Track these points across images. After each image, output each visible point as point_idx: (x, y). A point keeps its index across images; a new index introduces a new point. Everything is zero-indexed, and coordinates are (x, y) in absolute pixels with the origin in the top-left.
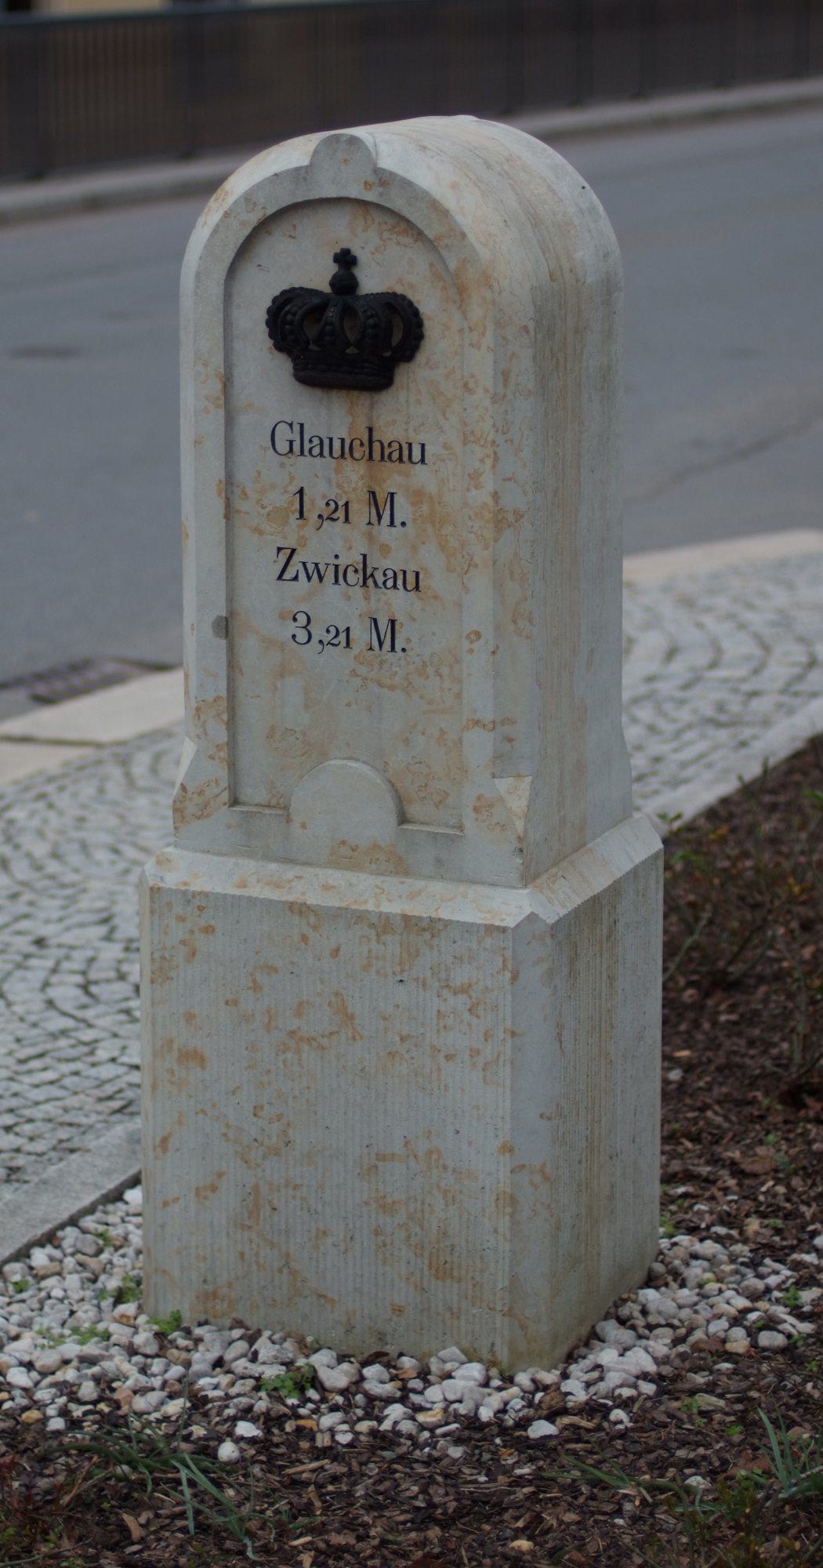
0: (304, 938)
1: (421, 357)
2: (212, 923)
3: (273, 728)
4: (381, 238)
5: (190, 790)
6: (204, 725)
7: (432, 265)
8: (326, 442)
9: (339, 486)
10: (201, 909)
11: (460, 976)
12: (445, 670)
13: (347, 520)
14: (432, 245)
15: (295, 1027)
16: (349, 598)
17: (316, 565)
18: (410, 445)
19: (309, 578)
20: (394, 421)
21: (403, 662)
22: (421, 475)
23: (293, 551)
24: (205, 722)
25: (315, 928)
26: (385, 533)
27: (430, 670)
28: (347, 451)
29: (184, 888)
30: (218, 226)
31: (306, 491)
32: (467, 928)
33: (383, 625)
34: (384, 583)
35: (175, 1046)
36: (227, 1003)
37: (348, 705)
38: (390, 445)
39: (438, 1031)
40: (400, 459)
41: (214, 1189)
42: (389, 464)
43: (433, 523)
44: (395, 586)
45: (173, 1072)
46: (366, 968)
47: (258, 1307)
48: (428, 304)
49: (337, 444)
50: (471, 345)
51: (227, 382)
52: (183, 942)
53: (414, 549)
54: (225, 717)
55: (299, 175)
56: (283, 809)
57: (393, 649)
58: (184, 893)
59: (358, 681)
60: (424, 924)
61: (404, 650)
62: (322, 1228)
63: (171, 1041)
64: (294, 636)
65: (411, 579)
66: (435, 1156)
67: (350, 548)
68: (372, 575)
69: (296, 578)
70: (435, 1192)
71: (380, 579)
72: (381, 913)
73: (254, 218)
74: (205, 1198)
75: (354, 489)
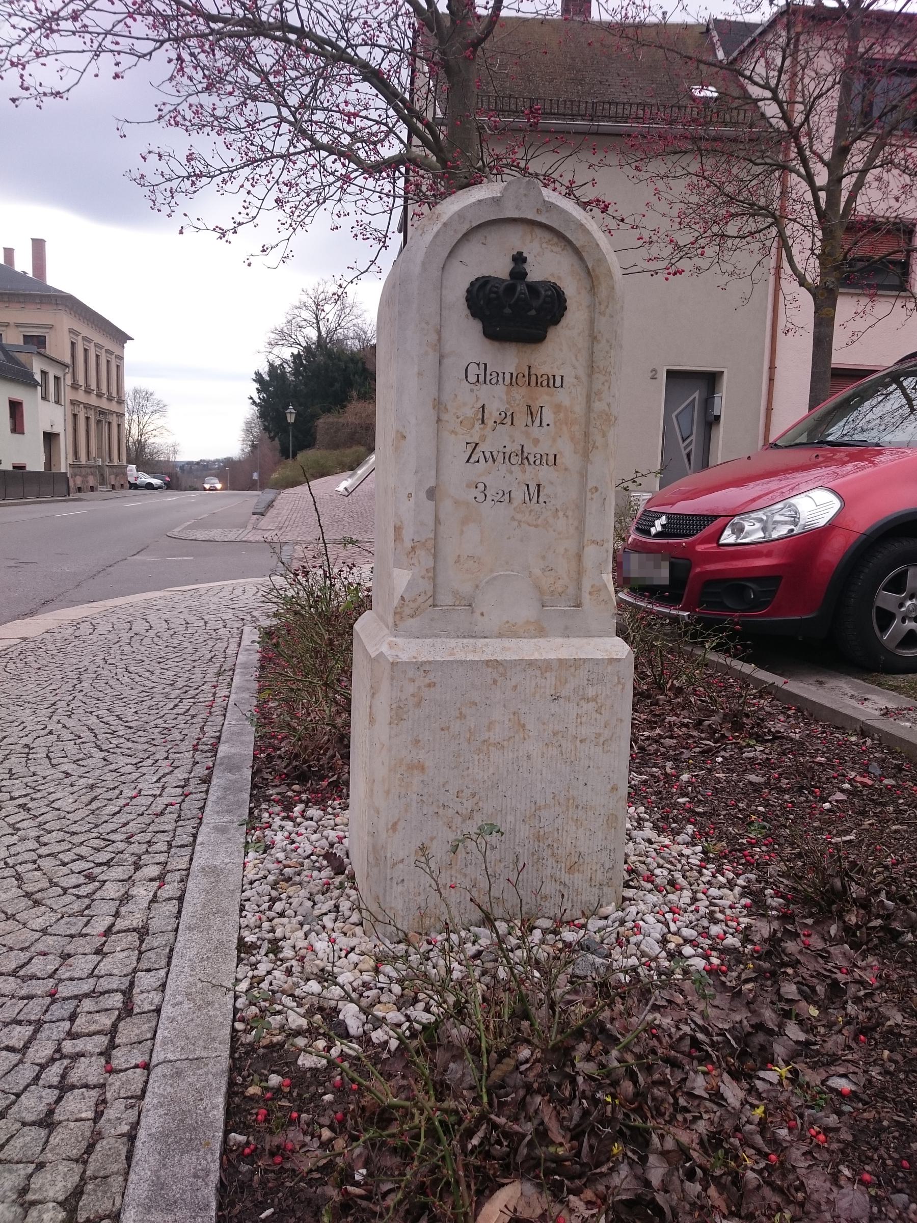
0: (495, 682)
1: (563, 322)
11: (591, 692)
16: (511, 472)
22: (562, 396)
25: (502, 675)
26: (535, 431)
27: (561, 514)
28: (514, 381)
32: (597, 662)
40: (548, 385)
48: (571, 289)
49: (508, 376)
52: (413, 695)
53: (554, 440)
60: (572, 663)
65: (551, 457)
71: (532, 460)
73: (465, 228)
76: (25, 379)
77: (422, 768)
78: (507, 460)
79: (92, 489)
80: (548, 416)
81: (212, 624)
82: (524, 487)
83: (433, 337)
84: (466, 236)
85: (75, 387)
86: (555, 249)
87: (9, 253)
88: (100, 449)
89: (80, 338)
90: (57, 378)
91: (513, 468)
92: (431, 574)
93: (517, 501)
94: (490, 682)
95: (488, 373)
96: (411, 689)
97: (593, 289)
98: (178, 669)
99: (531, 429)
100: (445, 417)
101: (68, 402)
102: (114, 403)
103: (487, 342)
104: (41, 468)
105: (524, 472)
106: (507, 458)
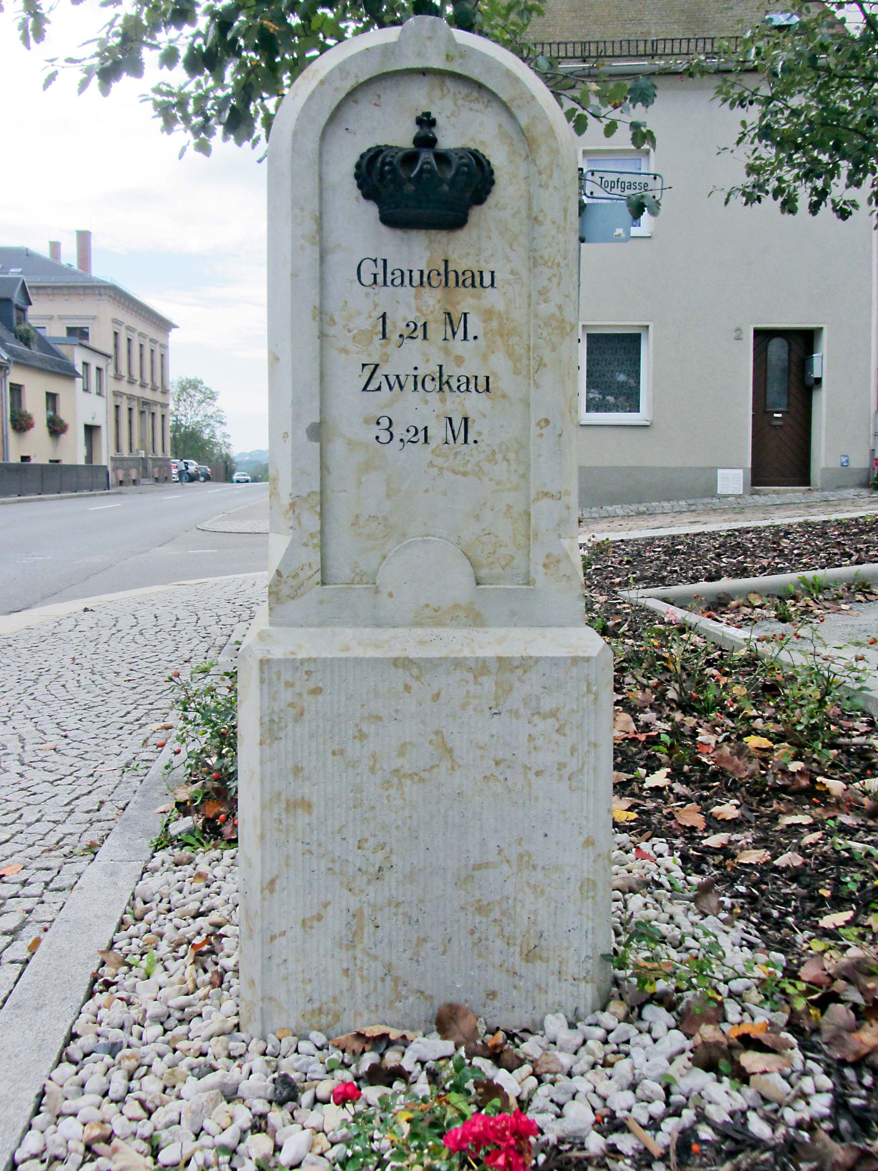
0: (407, 688)
1: (491, 200)
2: (320, 685)
3: (357, 516)
4: (456, 105)
5: (285, 574)
6: (298, 518)
7: (500, 126)
8: (407, 274)
9: (418, 309)
10: (308, 673)
11: (547, 704)
12: (512, 456)
13: (425, 337)
14: (506, 107)
15: (399, 765)
16: (426, 402)
17: (397, 376)
18: (481, 272)
19: (391, 388)
20: (468, 254)
21: (475, 452)
22: (491, 298)
23: (377, 366)
24: (299, 514)
25: (418, 678)
26: (458, 345)
27: (499, 457)
28: (425, 280)
29: (292, 657)
30: (313, 92)
31: (388, 315)
32: (555, 662)
33: (457, 423)
34: (458, 387)
35: (283, 798)
36: (334, 753)
37: (426, 491)
38: (463, 273)
39: (529, 753)
40: (473, 285)
41: (319, 918)
42: (463, 289)
43: (502, 336)
44: (468, 390)
45: (280, 821)
46: (464, 707)
47: (361, 1015)
48: (498, 157)
49: (416, 275)
50: (541, 186)
51: (320, 220)
52: (292, 705)
53: (485, 358)
54: (318, 509)
55: (387, 50)
56: (370, 581)
57: (466, 442)
58: (294, 660)
59: (434, 471)
60: (516, 663)
61: (475, 442)
62: (422, 935)
63: (279, 794)
64: (377, 438)
65: (482, 382)
66: (526, 858)
67: (428, 361)
68: (447, 382)
69: (379, 389)
70: (527, 889)
71: (454, 384)
72: (477, 659)
74: (311, 927)
75: (432, 312)
76: (67, 372)
77: (308, 806)
78: (419, 386)
79: (135, 482)
80: (475, 326)
81: (205, 620)
82: (445, 421)
83: (310, 227)
84: (352, 94)
85: (118, 377)
86: (475, 106)
87: (55, 247)
88: (142, 441)
89: (136, 334)
90: (99, 369)
91: (429, 397)
92: (316, 541)
93: (434, 443)
94: (401, 688)
95: (389, 271)
96: (286, 696)
97: (530, 156)
98: (147, 671)
99: (451, 342)
100: (332, 331)
101: (110, 394)
102: (158, 393)
103: (384, 230)
104: (81, 461)
105: (443, 401)
106: (419, 383)
